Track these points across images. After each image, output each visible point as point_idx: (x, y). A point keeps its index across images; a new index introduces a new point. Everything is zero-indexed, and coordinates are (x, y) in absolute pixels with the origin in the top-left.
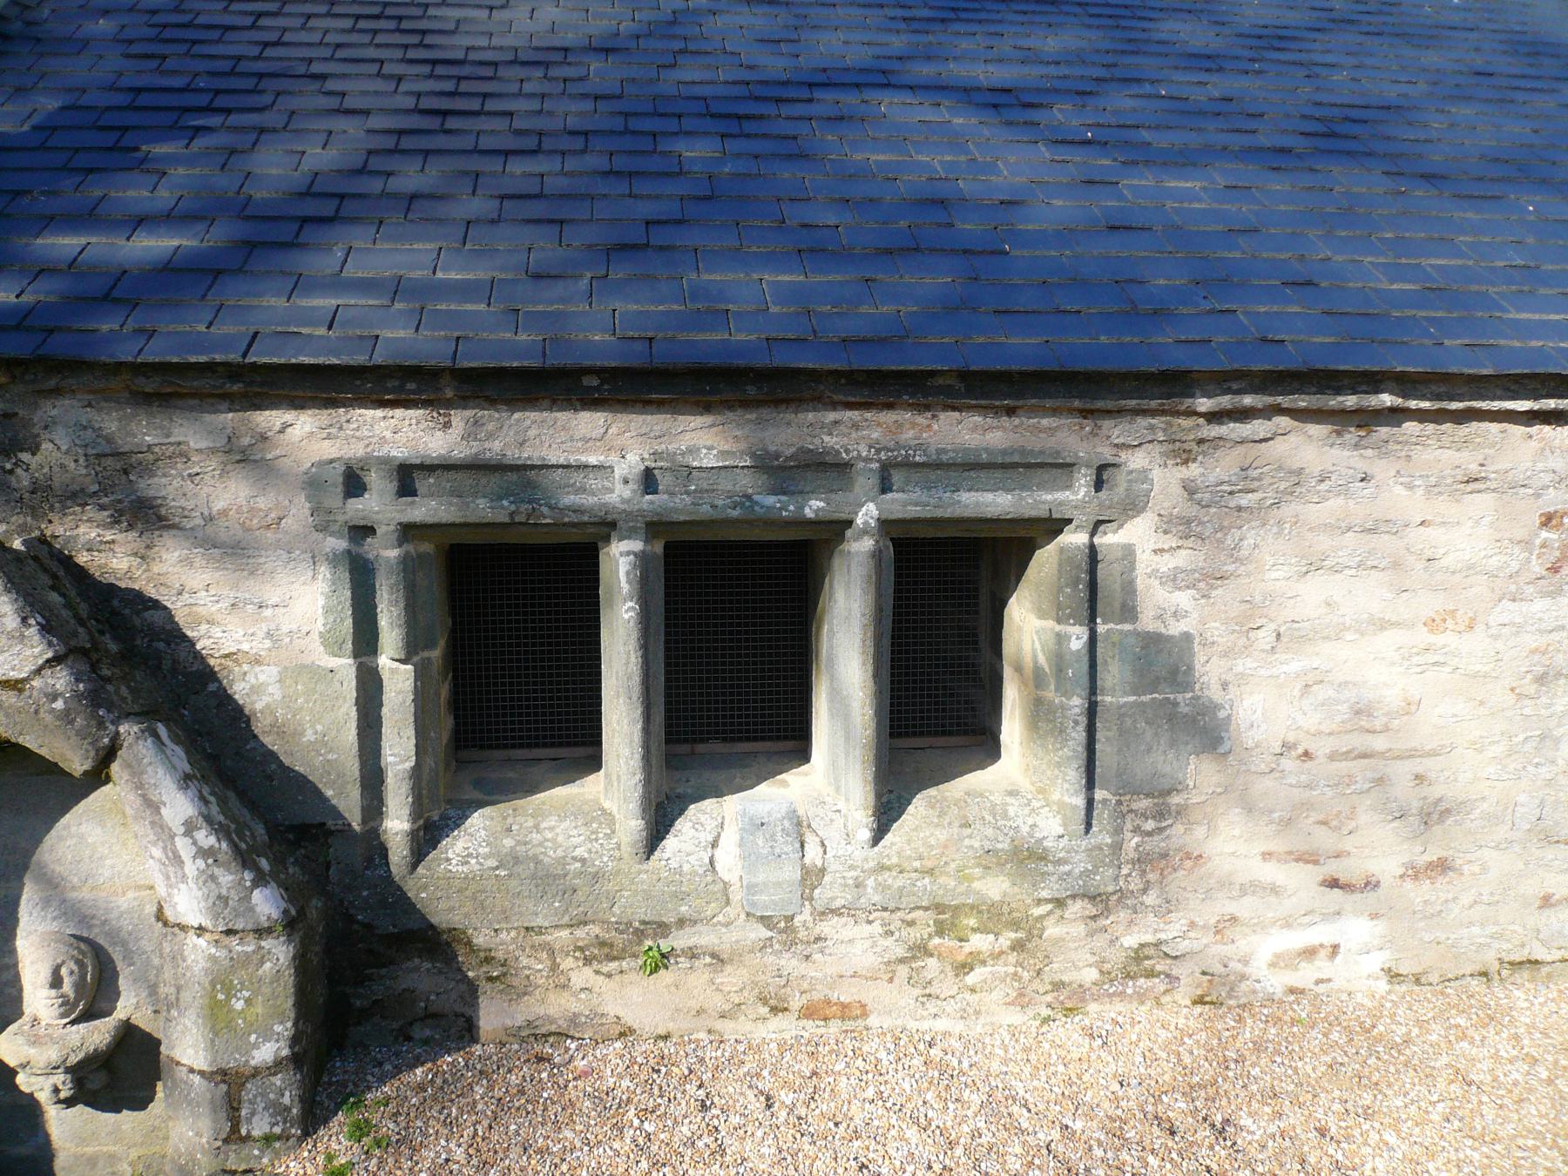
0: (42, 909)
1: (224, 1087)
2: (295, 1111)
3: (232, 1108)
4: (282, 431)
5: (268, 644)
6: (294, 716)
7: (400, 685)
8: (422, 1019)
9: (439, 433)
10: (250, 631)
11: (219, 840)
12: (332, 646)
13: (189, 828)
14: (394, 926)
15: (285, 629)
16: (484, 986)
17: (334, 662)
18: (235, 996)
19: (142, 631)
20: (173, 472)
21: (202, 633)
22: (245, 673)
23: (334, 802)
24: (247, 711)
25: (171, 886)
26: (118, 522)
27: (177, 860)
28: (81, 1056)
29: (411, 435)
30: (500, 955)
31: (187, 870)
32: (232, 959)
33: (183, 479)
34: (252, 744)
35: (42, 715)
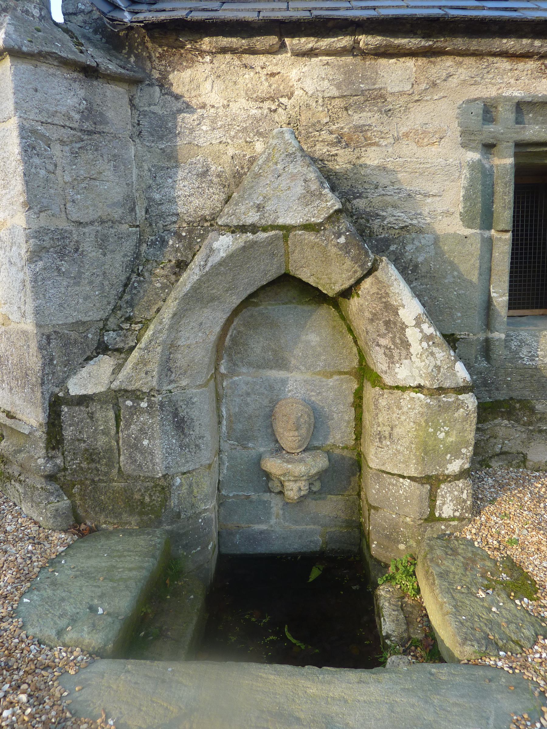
2: (469, 502)
8: (498, 455)
11: (435, 330)
14: (490, 398)
18: (440, 430)
20: (376, 108)
25: (393, 363)
29: (526, 81)
31: (412, 350)
32: (440, 406)
33: (381, 113)
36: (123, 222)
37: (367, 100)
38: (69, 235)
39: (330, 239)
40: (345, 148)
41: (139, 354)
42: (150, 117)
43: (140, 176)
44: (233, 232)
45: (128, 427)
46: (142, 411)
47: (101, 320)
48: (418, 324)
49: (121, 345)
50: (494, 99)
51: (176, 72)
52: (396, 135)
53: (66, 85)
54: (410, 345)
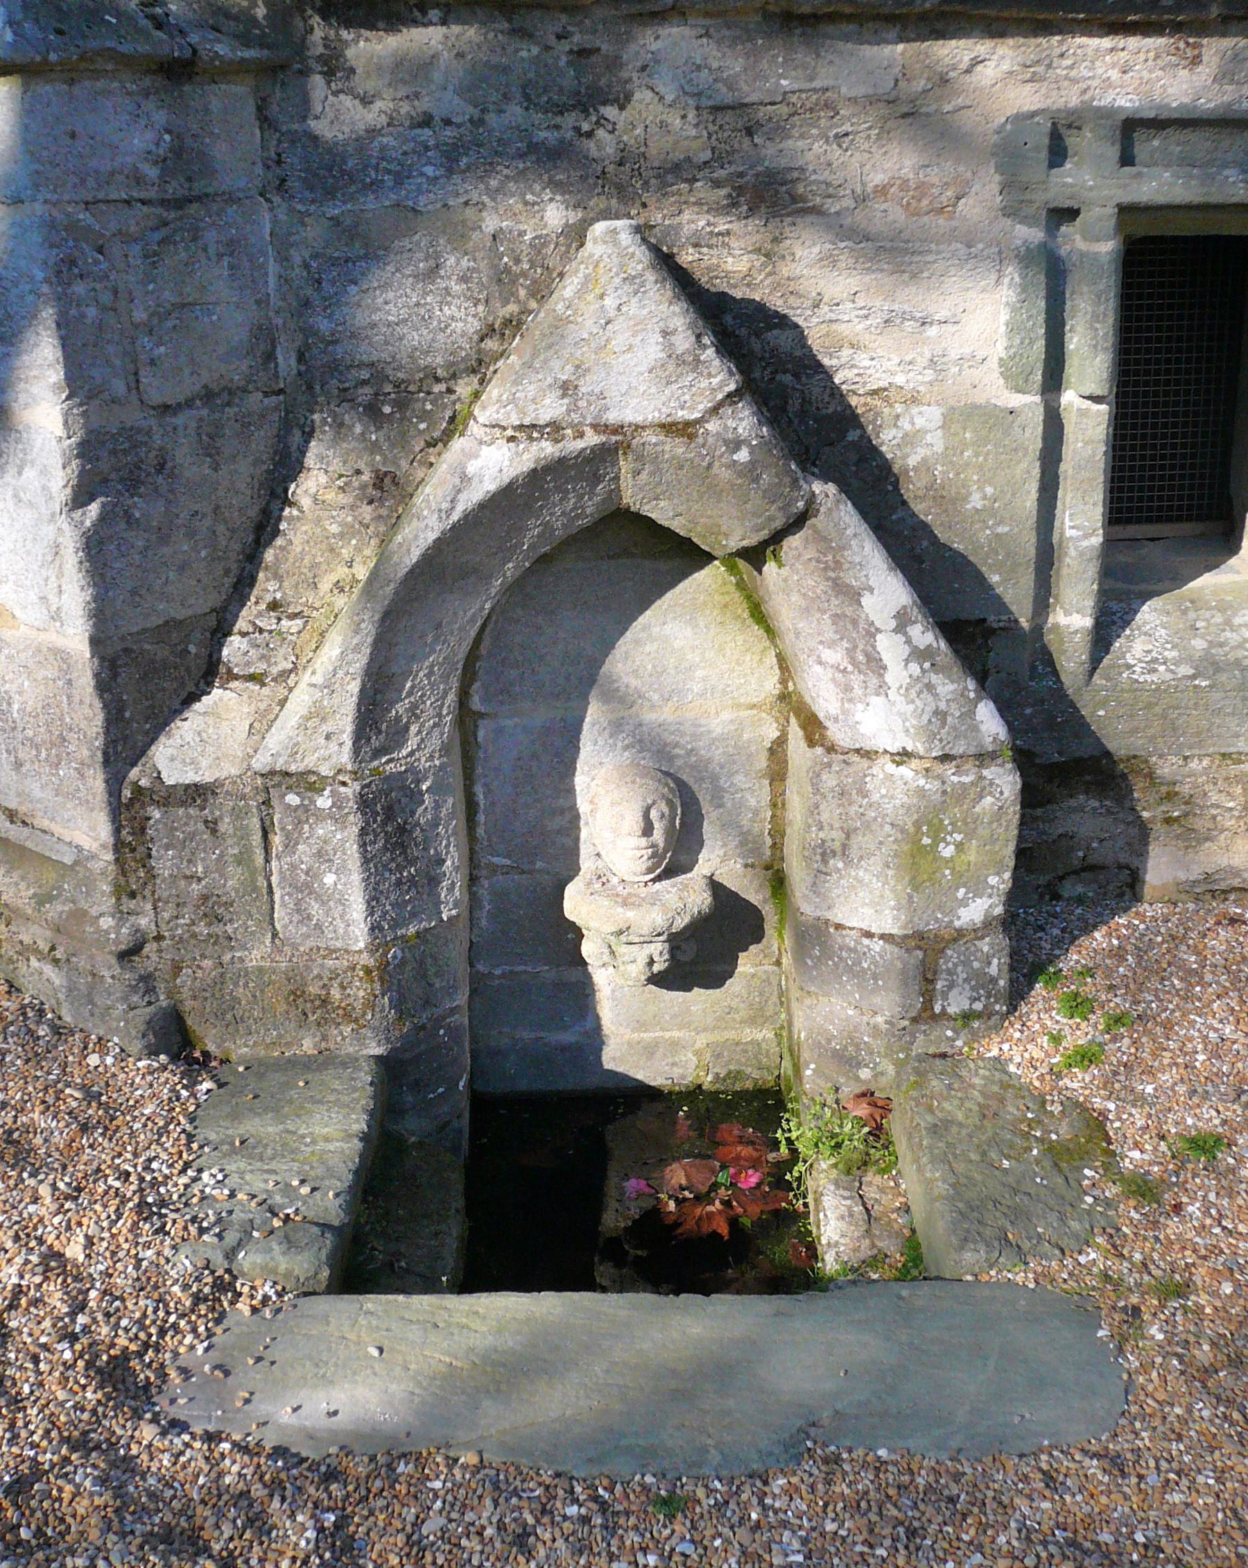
0: (611, 736)
1: (920, 954)
2: (1002, 983)
3: (926, 980)
4: (968, 71)
5: (929, 375)
6: (958, 474)
7: (1090, 432)
8: (1076, 872)
9: (1184, 73)
10: (908, 358)
12: (1014, 378)
13: (902, 622)
15: (954, 354)
16: (1158, 828)
17: (1017, 400)
18: (944, 840)
19: (762, 359)
20: (814, 131)
21: (843, 360)
22: (898, 416)
23: (999, 590)
24: (896, 469)
25: (850, 700)
26: (735, 204)
27: (876, 665)
28: (687, 920)
29: (1145, 74)
30: (1185, 789)
31: (889, 678)
32: (944, 792)
33: (827, 142)
34: (900, 514)
35: (716, 469)
36: (251, 387)
37: (795, 113)
38: (146, 439)
39: (718, 453)
40: (746, 218)
41: (311, 696)
42: (304, 147)
43: (284, 280)
44: (511, 439)
45: (290, 845)
46: (320, 816)
47: (213, 610)
48: (901, 628)
49: (260, 667)
50: (1071, 112)
51: (362, 43)
52: (859, 191)
53: (129, 108)
54: (885, 668)
